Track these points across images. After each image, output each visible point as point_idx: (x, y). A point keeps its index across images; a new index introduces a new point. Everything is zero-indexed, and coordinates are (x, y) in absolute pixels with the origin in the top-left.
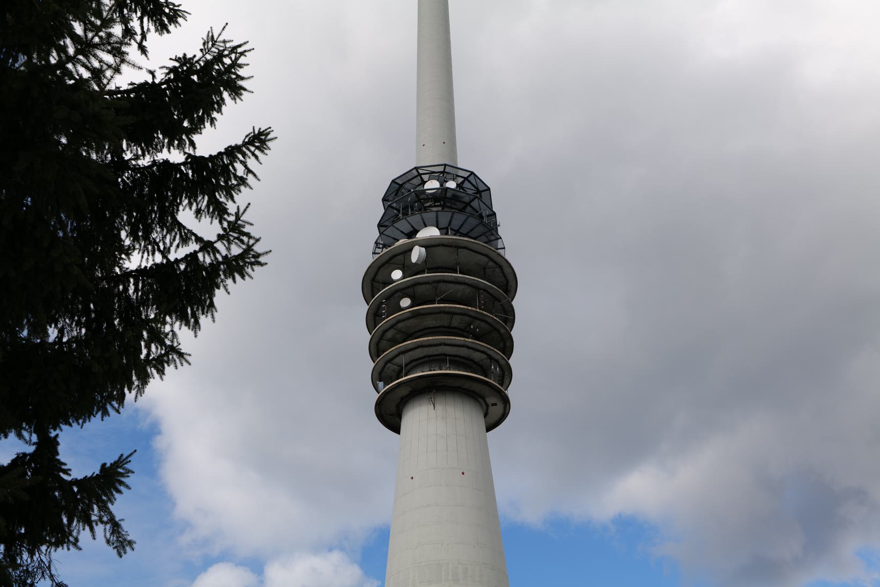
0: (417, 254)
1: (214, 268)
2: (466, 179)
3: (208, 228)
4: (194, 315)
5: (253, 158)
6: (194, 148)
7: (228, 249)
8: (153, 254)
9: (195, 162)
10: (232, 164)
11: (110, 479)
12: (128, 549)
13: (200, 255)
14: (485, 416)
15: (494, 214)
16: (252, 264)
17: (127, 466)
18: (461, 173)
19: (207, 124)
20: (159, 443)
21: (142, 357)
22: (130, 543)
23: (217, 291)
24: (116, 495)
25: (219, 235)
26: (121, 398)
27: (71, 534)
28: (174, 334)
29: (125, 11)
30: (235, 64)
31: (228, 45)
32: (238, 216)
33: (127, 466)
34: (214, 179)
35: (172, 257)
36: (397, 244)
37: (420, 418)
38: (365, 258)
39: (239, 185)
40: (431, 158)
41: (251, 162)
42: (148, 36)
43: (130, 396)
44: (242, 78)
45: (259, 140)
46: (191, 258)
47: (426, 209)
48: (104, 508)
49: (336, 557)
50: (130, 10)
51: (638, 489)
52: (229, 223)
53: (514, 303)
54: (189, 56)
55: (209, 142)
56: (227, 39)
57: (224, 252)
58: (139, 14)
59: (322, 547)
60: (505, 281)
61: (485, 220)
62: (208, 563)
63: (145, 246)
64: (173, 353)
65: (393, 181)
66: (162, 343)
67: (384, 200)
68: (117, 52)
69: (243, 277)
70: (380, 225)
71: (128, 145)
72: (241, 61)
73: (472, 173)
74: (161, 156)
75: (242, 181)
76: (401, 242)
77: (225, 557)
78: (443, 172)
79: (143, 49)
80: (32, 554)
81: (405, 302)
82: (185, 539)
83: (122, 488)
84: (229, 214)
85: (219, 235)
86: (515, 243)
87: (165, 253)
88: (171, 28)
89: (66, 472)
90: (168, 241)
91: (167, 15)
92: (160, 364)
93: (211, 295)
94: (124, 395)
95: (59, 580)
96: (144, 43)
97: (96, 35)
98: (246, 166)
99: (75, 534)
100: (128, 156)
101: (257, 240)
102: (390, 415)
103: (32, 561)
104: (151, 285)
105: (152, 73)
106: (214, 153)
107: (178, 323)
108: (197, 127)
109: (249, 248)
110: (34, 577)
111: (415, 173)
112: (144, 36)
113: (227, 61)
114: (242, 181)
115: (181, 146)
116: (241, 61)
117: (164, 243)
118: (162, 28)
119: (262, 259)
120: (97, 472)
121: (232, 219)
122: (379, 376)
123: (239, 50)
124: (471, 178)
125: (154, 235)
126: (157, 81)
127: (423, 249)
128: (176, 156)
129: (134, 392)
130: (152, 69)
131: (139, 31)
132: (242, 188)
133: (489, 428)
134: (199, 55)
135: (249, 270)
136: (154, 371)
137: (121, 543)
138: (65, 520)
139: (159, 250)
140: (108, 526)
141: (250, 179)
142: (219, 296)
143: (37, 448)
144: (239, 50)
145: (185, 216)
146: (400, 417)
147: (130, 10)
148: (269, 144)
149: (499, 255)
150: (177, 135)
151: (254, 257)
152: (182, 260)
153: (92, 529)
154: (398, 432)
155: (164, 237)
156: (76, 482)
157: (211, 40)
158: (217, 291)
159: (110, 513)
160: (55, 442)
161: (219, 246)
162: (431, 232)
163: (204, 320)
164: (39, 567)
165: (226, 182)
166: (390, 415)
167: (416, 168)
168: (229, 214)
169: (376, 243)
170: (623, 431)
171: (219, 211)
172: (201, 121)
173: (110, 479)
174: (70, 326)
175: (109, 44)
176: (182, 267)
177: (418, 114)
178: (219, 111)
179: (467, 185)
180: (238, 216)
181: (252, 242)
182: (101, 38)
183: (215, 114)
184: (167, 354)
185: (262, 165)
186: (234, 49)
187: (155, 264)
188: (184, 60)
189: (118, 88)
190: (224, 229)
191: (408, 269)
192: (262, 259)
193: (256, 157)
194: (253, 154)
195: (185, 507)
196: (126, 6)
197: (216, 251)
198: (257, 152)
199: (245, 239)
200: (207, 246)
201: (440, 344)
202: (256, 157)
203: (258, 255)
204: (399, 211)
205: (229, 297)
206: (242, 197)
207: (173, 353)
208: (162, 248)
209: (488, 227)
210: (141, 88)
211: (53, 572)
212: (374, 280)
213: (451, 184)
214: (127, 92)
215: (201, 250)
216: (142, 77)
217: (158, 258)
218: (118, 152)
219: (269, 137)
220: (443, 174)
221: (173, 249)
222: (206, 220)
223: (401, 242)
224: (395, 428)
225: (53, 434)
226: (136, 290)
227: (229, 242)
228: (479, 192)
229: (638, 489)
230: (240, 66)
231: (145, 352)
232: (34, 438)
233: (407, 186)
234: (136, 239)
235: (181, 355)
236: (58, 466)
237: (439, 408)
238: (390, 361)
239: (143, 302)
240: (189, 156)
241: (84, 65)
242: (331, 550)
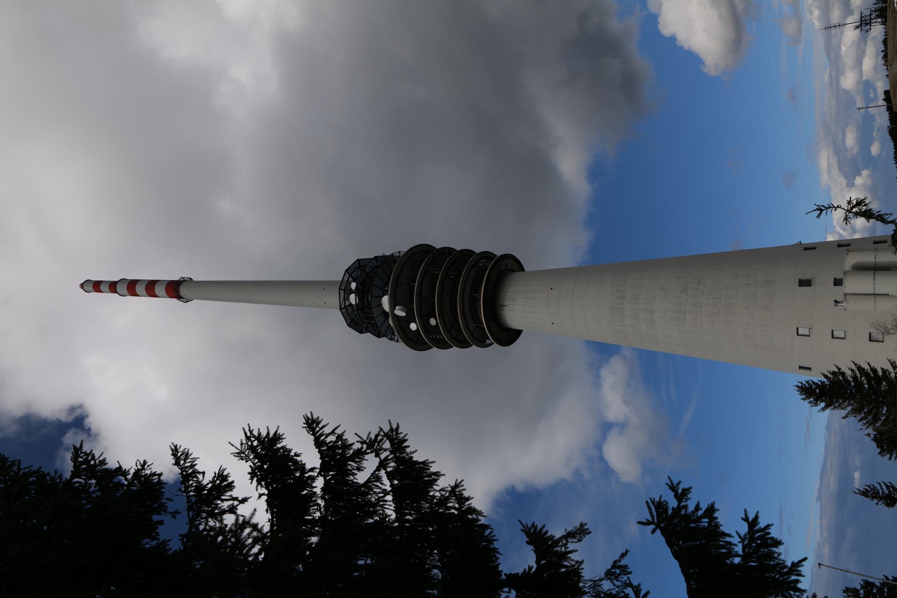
0: (400, 312)
1: (397, 460)
2: (350, 275)
3: (371, 463)
6: (315, 468)
7: (386, 450)
11: (537, 538)
13: (389, 469)
14: (513, 271)
15: (376, 257)
16: (397, 433)
17: (530, 525)
18: (346, 278)
19: (299, 459)
20: (520, 487)
22: (582, 525)
23: (414, 459)
24: (549, 534)
26: (485, 527)
27: (573, 566)
28: (442, 490)
30: (258, 438)
31: (244, 442)
32: (363, 442)
34: (337, 456)
35: (389, 489)
37: (515, 313)
38: (401, 347)
39: (342, 440)
40: (334, 299)
41: (327, 430)
42: (234, 496)
43: (483, 521)
44: (268, 434)
45: (312, 424)
46: (391, 476)
47: (369, 304)
48: (556, 542)
49: (604, 372)
51: (571, 163)
52: (367, 448)
54: (250, 470)
55: (311, 458)
57: (388, 453)
58: (219, 502)
59: (597, 383)
60: (422, 252)
61: (379, 264)
62: (602, 459)
64: (456, 492)
65: (349, 325)
67: (361, 332)
68: (246, 523)
69: (406, 440)
70: (379, 337)
72: (256, 433)
73: (346, 271)
74: (318, 491)
75: (340, 437)
77: (599, 447)
78: (345, 291)
79: (244, 500)
81: (433, 322)
82: (587, 475)
83: (544, 530)
84: (362, 448)
86: (396, 243)
87: (386, 493)
88: (230, 480)
90: (378, 491)
91: (221, 482)
92: (462, 500)
93: (417, 462)
94: (481, 524)
95: (603, 575)
96: (240, 499)
97: (230, 539)
98: (330, 434)
100: (318, 514)
101: (381, 429)
102: (509, 336)
103: (589, 593)
104: (407, 504)
105: (260, 496)
106: (319, 456)
108: (301, 467)
109: (386, 435)
110: (600, 592)
111: (343, 310)
112: (236, 499)
113: (255, 443)
114: (340, 437)
115: (313, 479)
116: (256, 433)
117: (379, 493)
119: (394, 427)
120: (532, 547)
121: (365, 446)
122: (482, 343)
123: (249, 434)
124: (350, 272)
125: (373, 499)
126: (266, 492)
128: (319, 483)
129: (480, 518)
130: (257, 496)
131: (231, 502)
132: (344, 438)
134: (250, 463)
135: (402, 436)
137: (580, 532)
138: (563, 570)
139: (384, 497)
140: (570, 540)
141: (339, 431)
142: (417, 457)
144: (249, 434)
145: (361, 478)
146: (512, 329)
148: (315, 417)
152: (391, 482)
153: (571, 552)
154: (521, 331)
155: (375, 493)
156: (537, 562)
157: (240, 455)
158: (414, 459)
159: (561, 538)
161: (383, 456)
162: (385, 300)
163: (433, 469)
164: (594, 588)
165: (339, 449)
166: (509, 336)
167: (341, 309)
168: (362, 448)
169: (390, 339)
170: (531, 173)
171: (359, 455)
172: (296, 463)
173: (537, 538)
174: (431, 560)
175: (237, 531)
176: (396, 482)
178: (290, 451)
179: (354, 275)
180: (363, 442)
181: (382, 433)
182: (232, 537)
183: (292, 454)
184: (455, 495)
185: (330, 421)
186: (248, 438)
187: (393, 500)
188: (253, 474)
190: (372, 452)
192: (394, 427)
193: (324, 427)
194: (321, 428)
195: (565, 473)
196: (213, 511)
197: (386, 459)
198: (320, 426)
199: (380, 438)
200: (383, 465)
202: (324, 427)
203: (391, 429)
204: (369, 323)
205: (420, 450)
206: (350, 438)
207: (456, 492)
209: (383, 263)
210: (271, 505)
212: (416, 343)
213: (353, 286)
214: (272, 514)
215: (385, 469)
216: (262, 504)
217: (389, 498)
218: (314, 522)
220: (347, 291)
221: (384, 487)
222: (365, 464)
224: (519, 332)
225: (504, 577)
226: (410, 514)
227: (381, 449)
228: (360, 267)
229: (571, 163)
230: (260, 434)
231: (453, 511)
232: (506, 589)
233: (352, 316)
234: (375, 513)
235: (457, 486)
236: (526, 574)
237: (506, 302)
238: (472, 334)
239: (419, 509)
240: (319, 473)
241: (250, 549)
242: (599, 376)
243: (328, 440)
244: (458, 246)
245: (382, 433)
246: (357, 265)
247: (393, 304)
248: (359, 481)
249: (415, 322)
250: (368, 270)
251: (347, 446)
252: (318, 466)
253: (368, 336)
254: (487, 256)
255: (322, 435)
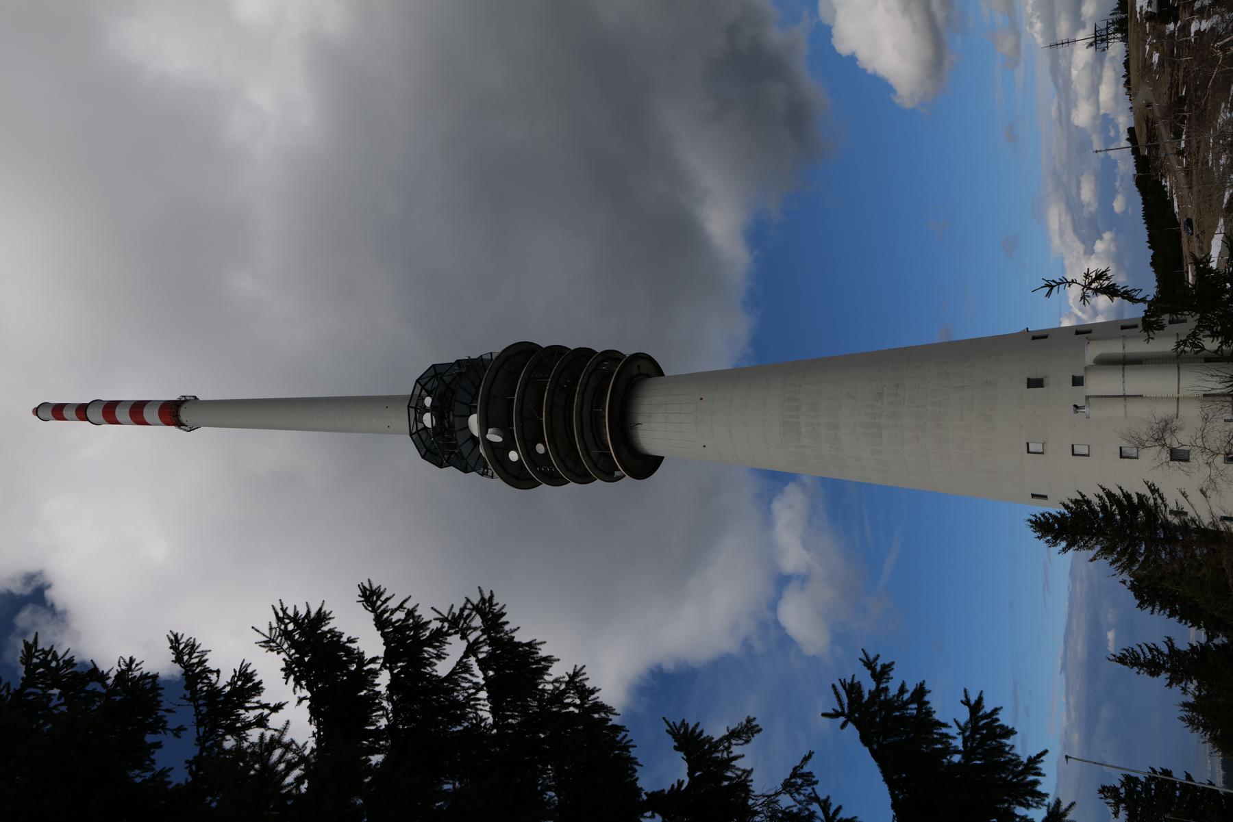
0: (494, 437)
1: (493, 642)
2: (423, 387)
3: (455, 647)
4: (538, 662)
5: (388, 603)
6: (377, 658)
7: (475, 629)
8: (479, 699)
9: (390, 659)
10: (393, 624)
11: (689, 741)
12: (754, 723)
13: (481, 656)
14: (649, 376)
15: (458, 361)
16: (491, 605)
17: (678, 724)
20: (669, 666)
21: (577, 711)
22: (749, 721)
23: (516, 640)
24: (705, 735)
25: (462, 638)
26: (617, 729)
27: (739, 777)
28: (556, 680)
29: (239, 725)
30: (295, 619)
31: (275, 625)
32: (443, 620)
33: (678, 724)
34: (407, 639)
36: (484, 455)
37: (653, 433)
38: (497, 485)
39: (413, 617)
40: (401, 420)
41: (392, 604)
42: (264, 702)
43: (615, 720)
44: (309, 612)
45: (370, 597)
46: (483, 665)
47: (451, 427)
48: (715, 746)
49: (777, 506)
50: (237, 720)
52: (449, 628)
53: (544, 344)
54: (283, 665)
55: (371, 644)
56: (268, 627)
57: (479, 633)
58: (242, 711)
59: (768, 521)
60: (522, 353)
63: (471, 707)
64: (575, 682)
65: (423, 457)
66: (564, 692)
67: (441, 466)
69: (503, 614)
70: (466, 471)
71: (372, 724)
72: (291, 612)
73: (417, 381)
75: (410, 613)
76: (482, 451)
78: (416, 409)
79: (277, 708)
80: (756, 813)
81: (540, 449)
82: (758, 645)
83: (698, 731)
85: (462, 638)
86: (485, 340)
87: (478, 688)
88: (257, 679)
89: (680, 783)
90: (467, 685)
91: (244, 684)
92: (584, 693)
93: (520, 644)
94: (613, 726)
95: (780, 788)
98: (396, 610)
99: (739, 773)
100: (383, 723)
101: (468, 600)
102: (645, 466)
105: (300, 700)
106: (382, 640)
107: (546, 677)
108: (359, 658)
109: (476, 608)
112: (266, 706)
113: (291, 627)
114: (410, 613)
115: (375, 673)
116: (291, 612)
118: (257, 689)
119: (487, 596)
121: (446, 625)
122: (609, 475)
123: (281, 615)
125: (461, 698)
126: (309, 695)
127: (490, 430)
128: (384, 679)
129: (611, 716)
130: (296, 700)
132: (417, 614)
133: (660, 373)
134: (283, 655)
135: (497, 608)
136: (592, 697)
137: (747, 731)
138: (726, 783)
139: (475, 694)
140: (734, 742)
141: (409, 605)
142: (521, 637)
143: (661, 814)
144: (281, 615)
145: (443, 669)
147: (237, 720)
148: (375, 586)
149: (497, 358)
150: (365, 678)
151: (484, 604)
152: (485, 674)
153: (736, 758)
155: (463, 688)
158: (516, 640)
159: (721, 740)
160: (652, 796)
161: (472, 638)
162: (473, 421)
163: (543, 652)
165: (410, 629)
166: (645, 466)
168: (443, 627)
169: (482, 475)
170: (667, 240)
172: (349, 652)
173: (689, 741)
176: (491, 673)
177: (359, 432)
179: (429, 387)
180: (443, 620)
181: (469, 606)
183: (344, 639)
184: (575, 687)
185: (396, 593)
188: (288, 671)
189: (314, 735)
190: (456, 633)
191: (508, 445)
192: (487, 596)
193: (387, 599)
198: (383, 598)
199: (466, 612)
200: (472, 650)
201: (581, 417)
202: (387, 599)
203: (483, 599)
206: (425, 614)
207: (575, 682)
208: (473, 691)
209: (469, 368)
211: (772, 792)
212: (518, 478)
213: (428, 401)
215: (475, 655)
216: (304, 711)
217: (483, 694)
219: (367, 586)
220: (420, 410)
221: (475, 680)
222: (447, 649)
223: (482, 451)
224: (658, 461)
226: (513, 717)
227: (469, 628)
228: (436, 376)
230: (296, 614)
231: (571, 709)
233: (428, 444)
235: (576, 674)
236: (675, 792)
237: (640, 419)
240: (383, 665)
243: (395, 618)
244: (572, 343)
245: (469, 606)
246: (432, 373)
247: (485, 425)
248: (439, 674)
249: (516, 450)
250: (447, 379)
251: (421, 626)
252: (382, 655)
253: (451, 470)
254: (611, 356)
255: (385, 611)
